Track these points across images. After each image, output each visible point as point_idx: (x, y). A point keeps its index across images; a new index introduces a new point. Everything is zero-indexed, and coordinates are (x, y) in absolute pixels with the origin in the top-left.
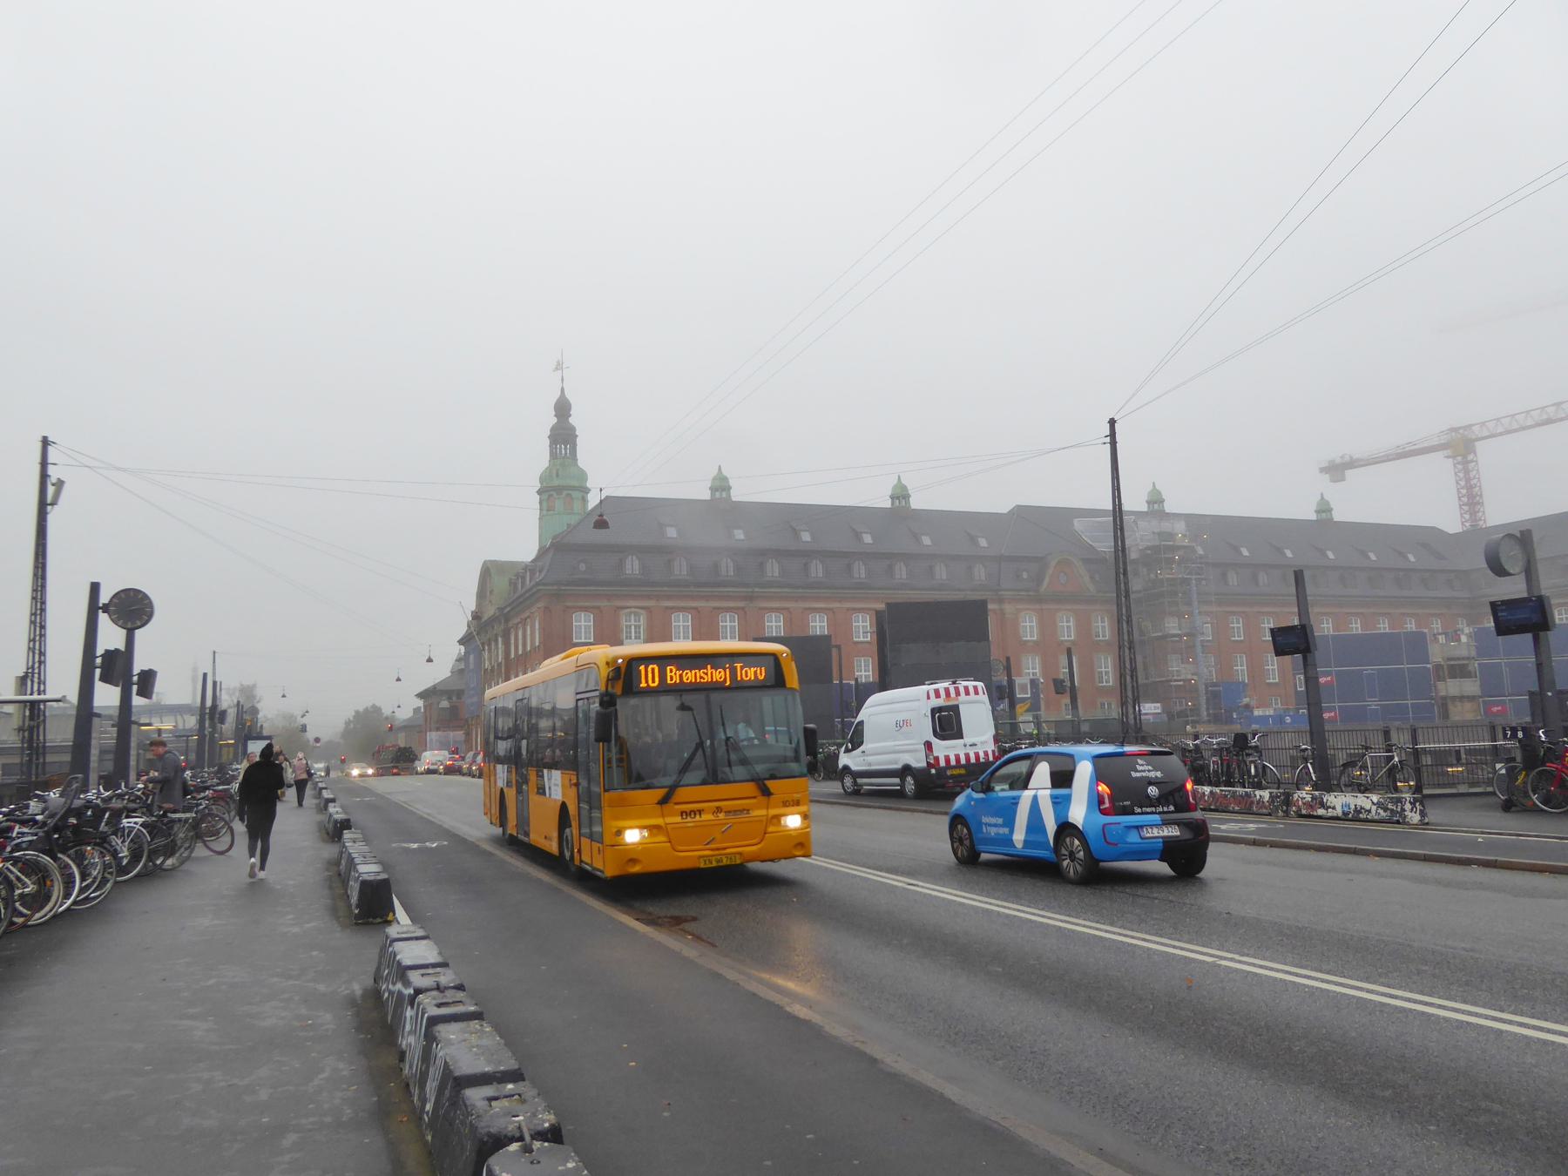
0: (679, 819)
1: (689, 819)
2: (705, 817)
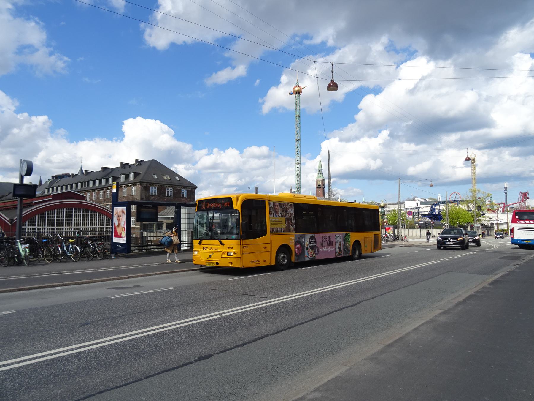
0: (202, 250)
1: (204, 250)
2: (208, 250)
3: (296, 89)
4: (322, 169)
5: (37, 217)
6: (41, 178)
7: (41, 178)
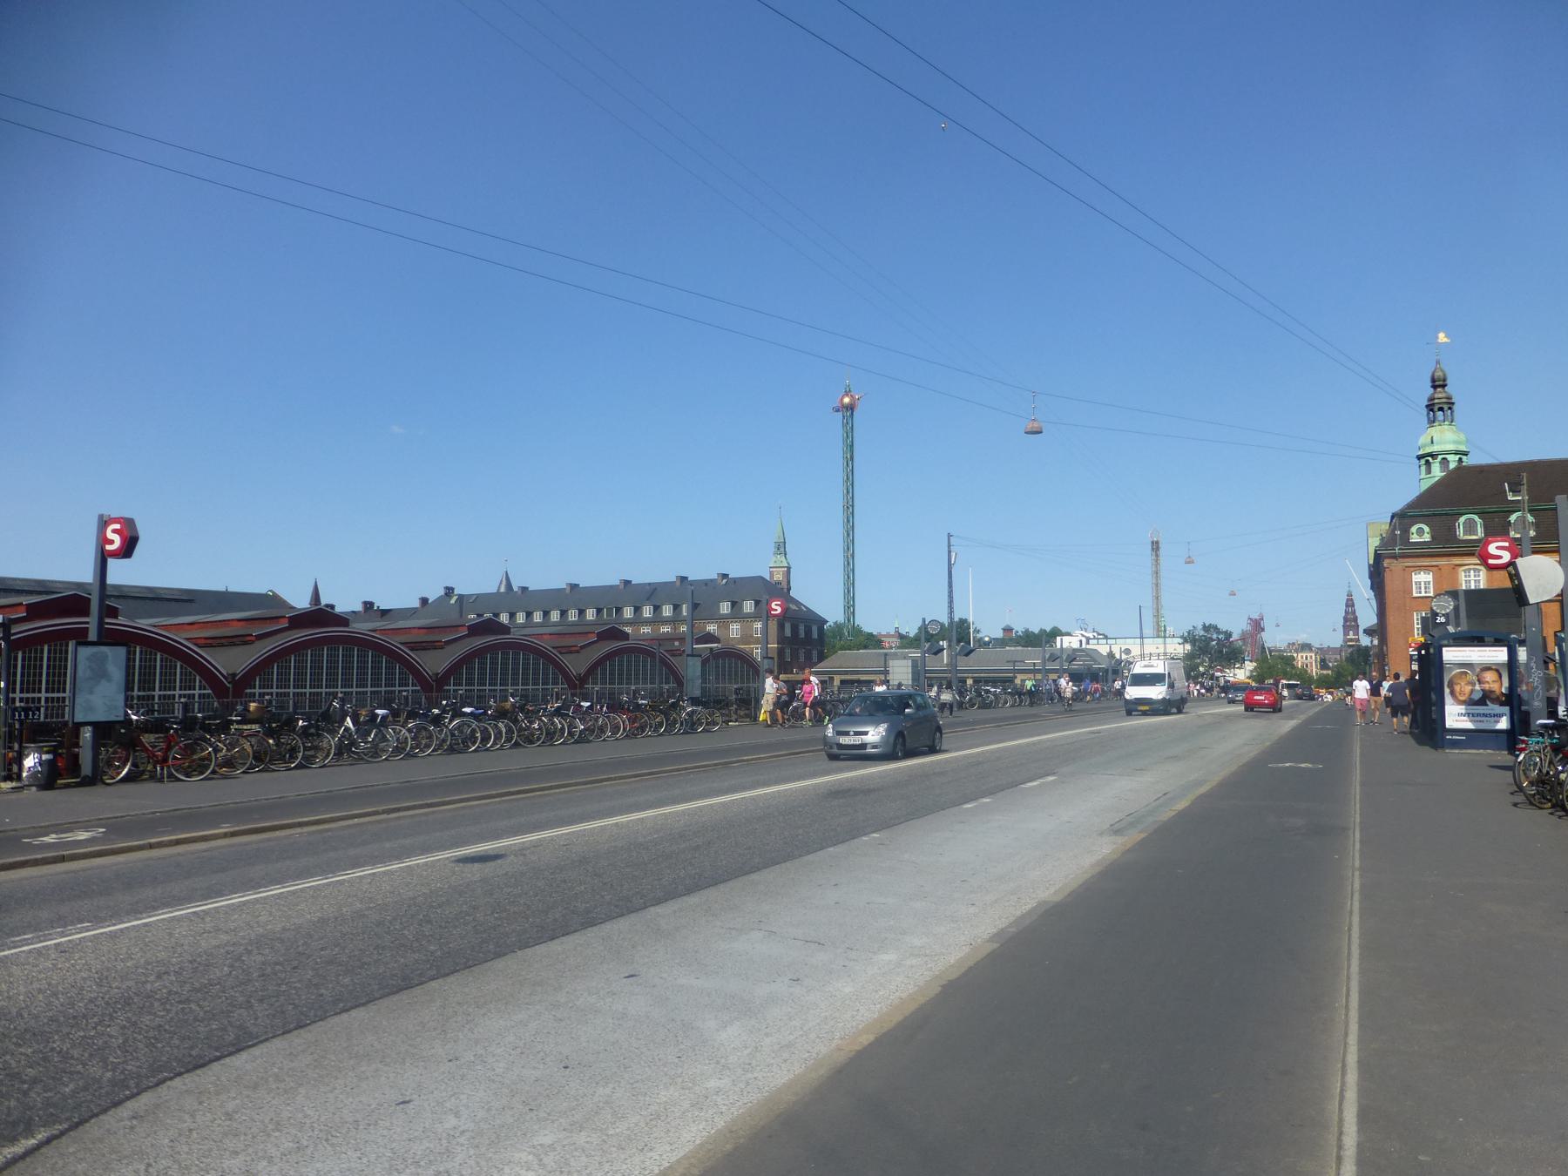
3: (847, 400)
4: (785, 543)
5: (275, 667)
6: (316, 582)
7: (316, 582)
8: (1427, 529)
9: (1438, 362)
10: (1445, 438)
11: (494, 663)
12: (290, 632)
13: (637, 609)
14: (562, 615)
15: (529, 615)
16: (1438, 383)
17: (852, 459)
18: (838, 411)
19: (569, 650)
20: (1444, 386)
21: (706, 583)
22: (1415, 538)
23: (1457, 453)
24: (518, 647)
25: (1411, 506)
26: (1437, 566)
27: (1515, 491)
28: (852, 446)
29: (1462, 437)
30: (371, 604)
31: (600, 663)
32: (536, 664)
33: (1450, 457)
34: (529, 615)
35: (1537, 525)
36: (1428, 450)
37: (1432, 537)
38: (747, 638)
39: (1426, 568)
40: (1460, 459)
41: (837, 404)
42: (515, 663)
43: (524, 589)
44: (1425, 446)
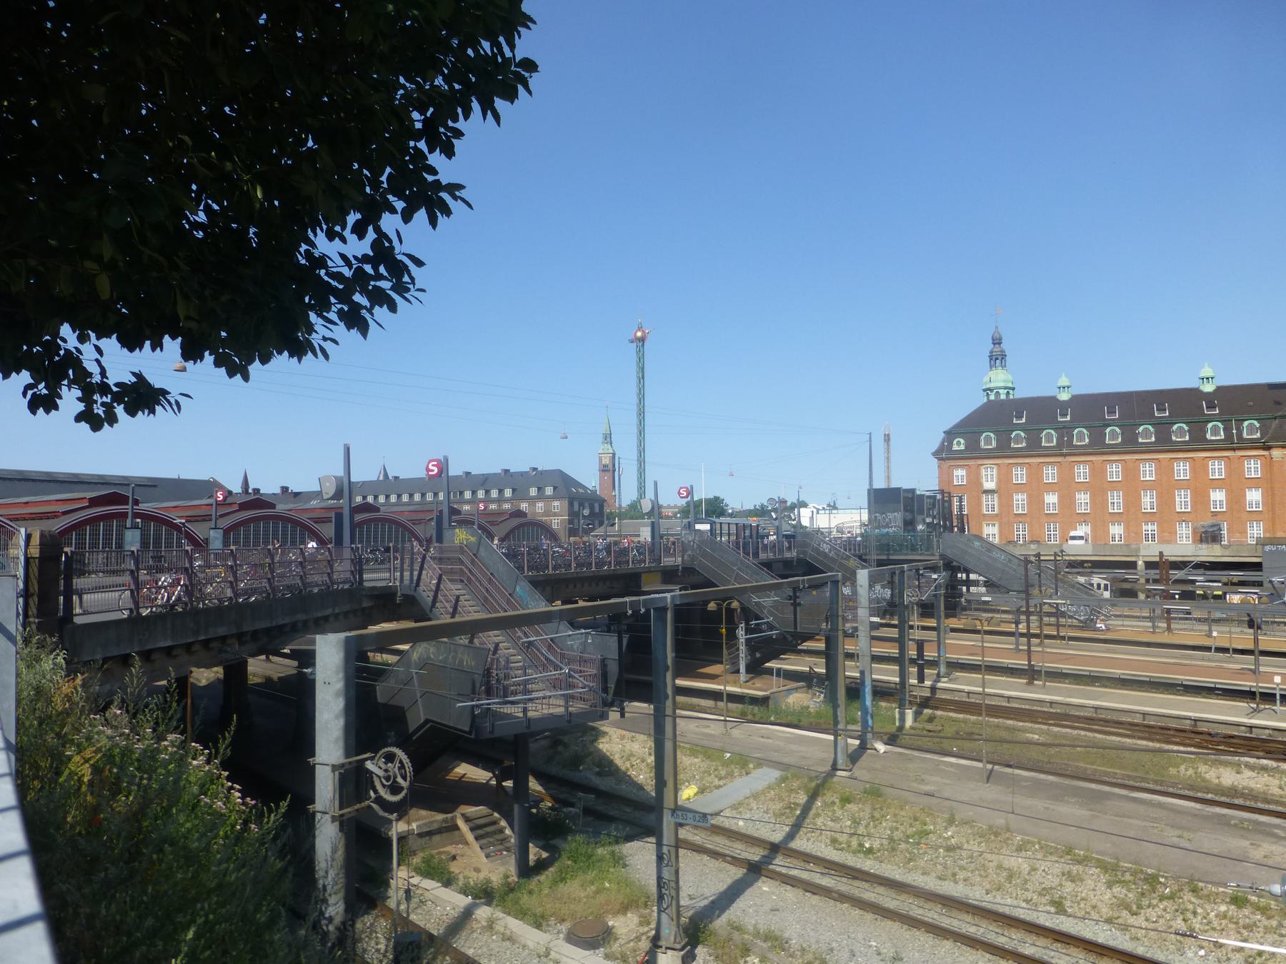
3: (639, 334)
8: (962, 441)
9: (997, 327)
10: (999, 378)
11: (368, 531)
12: (239, 513)
13: (474, 493)
14: (375, 499)
15: (399, 496)
16: (997, 341)
17: (643, 378)
18: (632, 342)
19: (492, 523)
20: (1000, 344)
21: (522, 474)
22: (955, 447)
23: (1005, 388)
24: (384, 520)
25: (957, 426)
26: (1157, 459)
27: (1162, 410)
28: (643, 368)
29: (1010, 377)
30: (287, 488)
31: (512, 531)
32: (397, 531)
33: (1001, 391)
34: (399, 496)
35: (1027, 439)
36: (988, 386)
37: (966, 447)
38: (548, 513)
39: (962, 466)
40: (1008, 392)
41: (632, 337)
42: (383, 531)
43: (396, 478)
44: (986, 383)
